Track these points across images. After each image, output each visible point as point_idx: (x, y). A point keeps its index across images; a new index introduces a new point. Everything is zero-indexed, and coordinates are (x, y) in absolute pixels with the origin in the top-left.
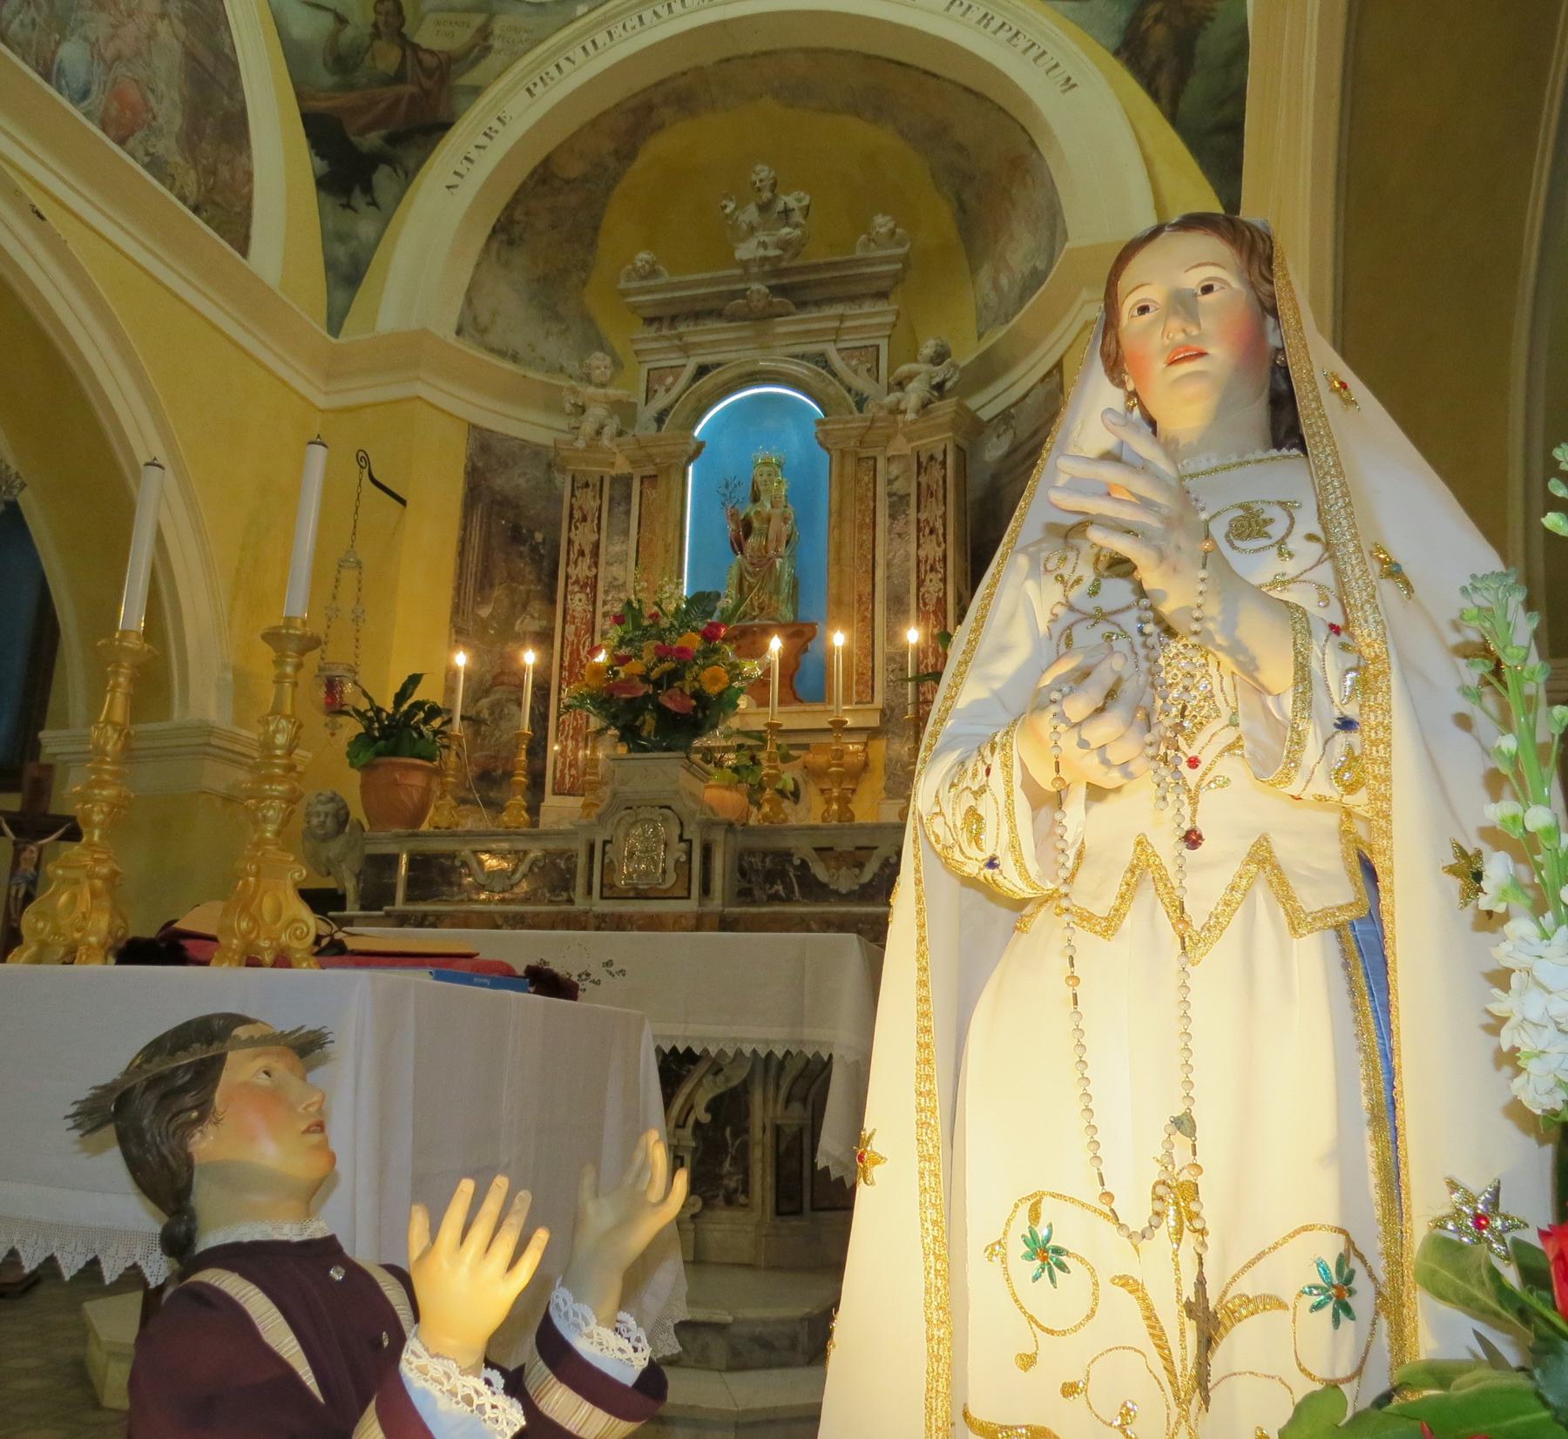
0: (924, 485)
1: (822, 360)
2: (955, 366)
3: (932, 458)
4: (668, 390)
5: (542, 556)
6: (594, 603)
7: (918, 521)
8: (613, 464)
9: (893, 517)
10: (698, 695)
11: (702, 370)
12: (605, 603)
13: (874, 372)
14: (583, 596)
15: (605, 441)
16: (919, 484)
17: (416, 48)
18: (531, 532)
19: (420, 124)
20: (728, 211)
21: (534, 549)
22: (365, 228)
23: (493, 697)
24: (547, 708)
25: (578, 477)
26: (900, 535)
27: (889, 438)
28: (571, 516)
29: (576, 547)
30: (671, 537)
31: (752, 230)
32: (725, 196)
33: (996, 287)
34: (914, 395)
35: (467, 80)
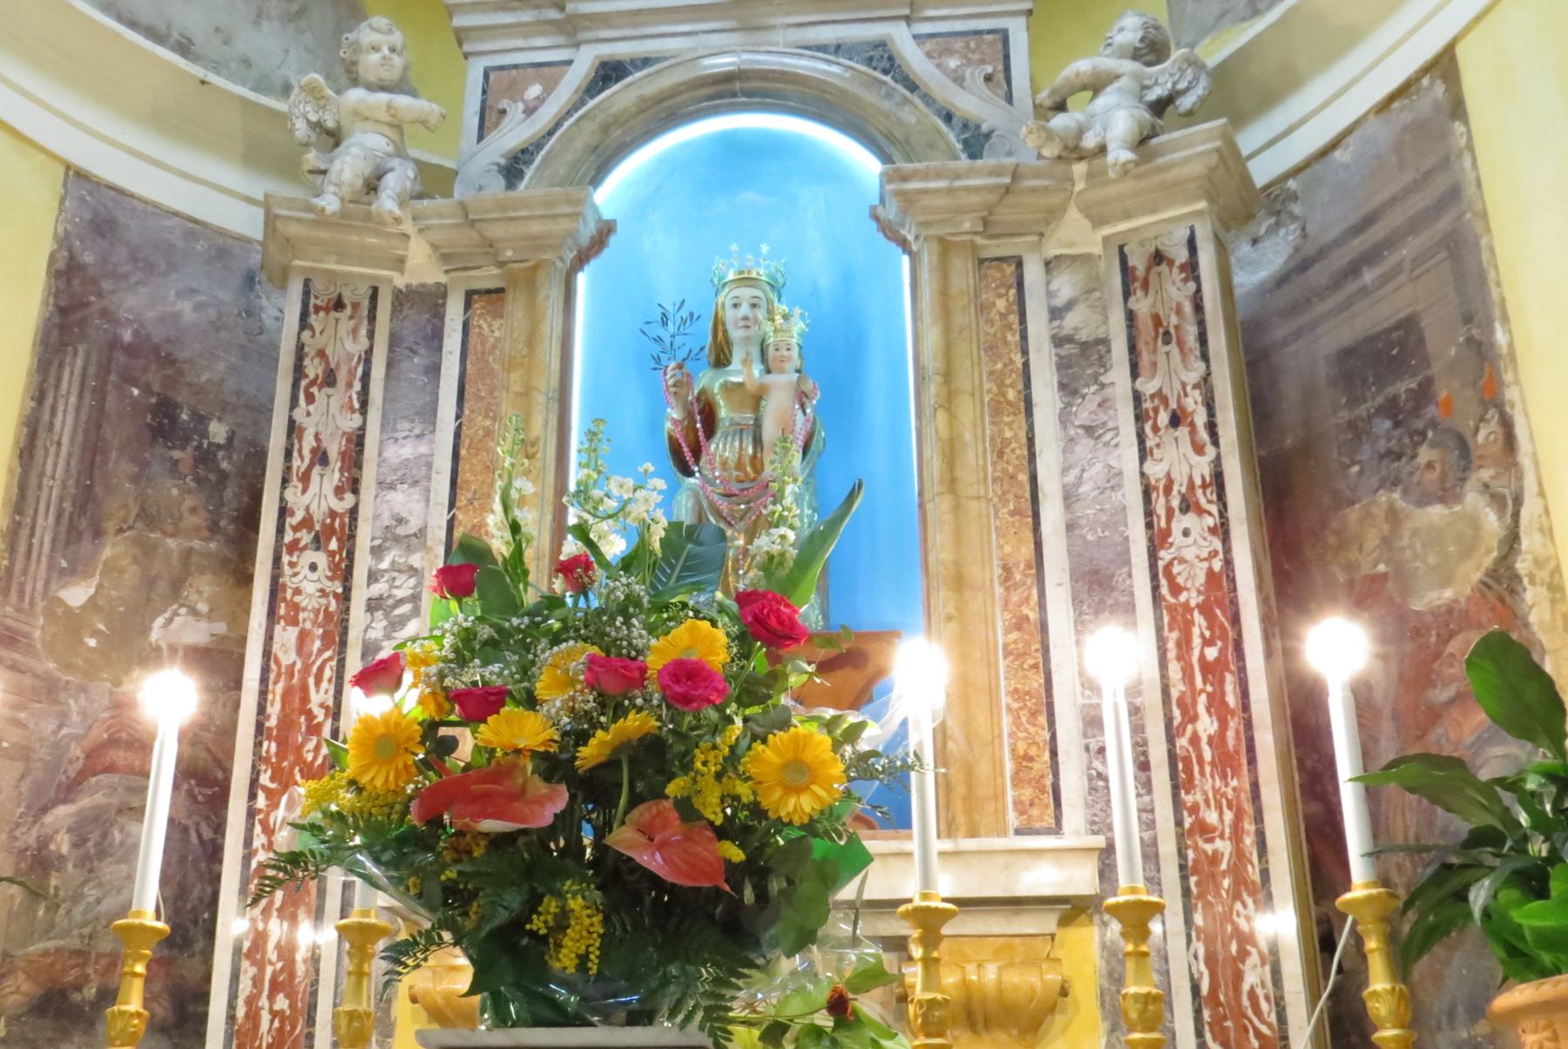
0: (1144, 322)
1: (883, 58)
2: (1194, 63)
3: (1158, 257)
4: (530, 111)
5: (223, 476)
7: (1137, 397)
8: (399, 263)
9: (1068, 388)
10: (748, 824)
12: (373, 577)
13: (1001, 80)
14: (321, 559)
15: (387, 202)
16: (1131, 317)
18: (201, 419)
21: (205, 457)
23: (85, 802)
24: (220, 829)
25: (318, 285)
26: (1089, 430)
27: (1054, 214)
28: (299, 371)
29: (308, 442)
30: (541, 424)
34: (1114, 120)
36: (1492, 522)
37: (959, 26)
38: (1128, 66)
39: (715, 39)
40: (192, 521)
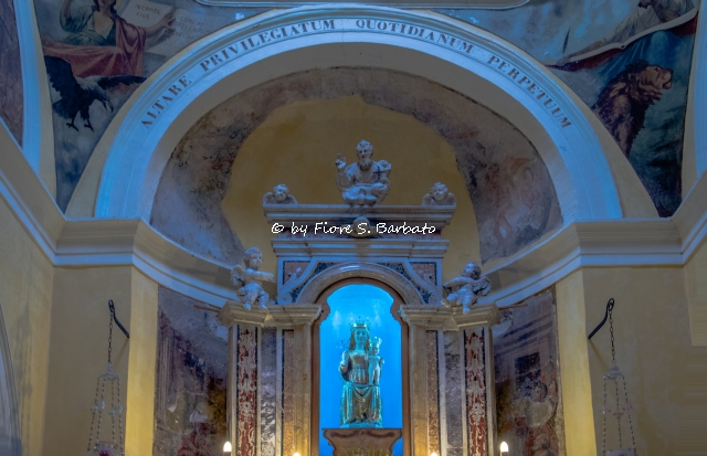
1: (400, 268)
3: (474, 335)
4: (298, 276)
6: (256, 409)
7: (466, 372)
9: (448, 368)
11: (322, 267)
14: (249, 403)
16: (466, 350)
17: (122, 20)
19: (123, 79)
20: (340, 166)
22: (83, 141)
25: (241, 327)
28: (238, 351)
29: (242, 372)
31: (354, 180)
32: (339, 157)
33: (497, 233)
35: (155, 50)
36: (550, 408)
37: (423, 260)
38: (470, 280)
39: (352, 259)
40: (196, 387)
